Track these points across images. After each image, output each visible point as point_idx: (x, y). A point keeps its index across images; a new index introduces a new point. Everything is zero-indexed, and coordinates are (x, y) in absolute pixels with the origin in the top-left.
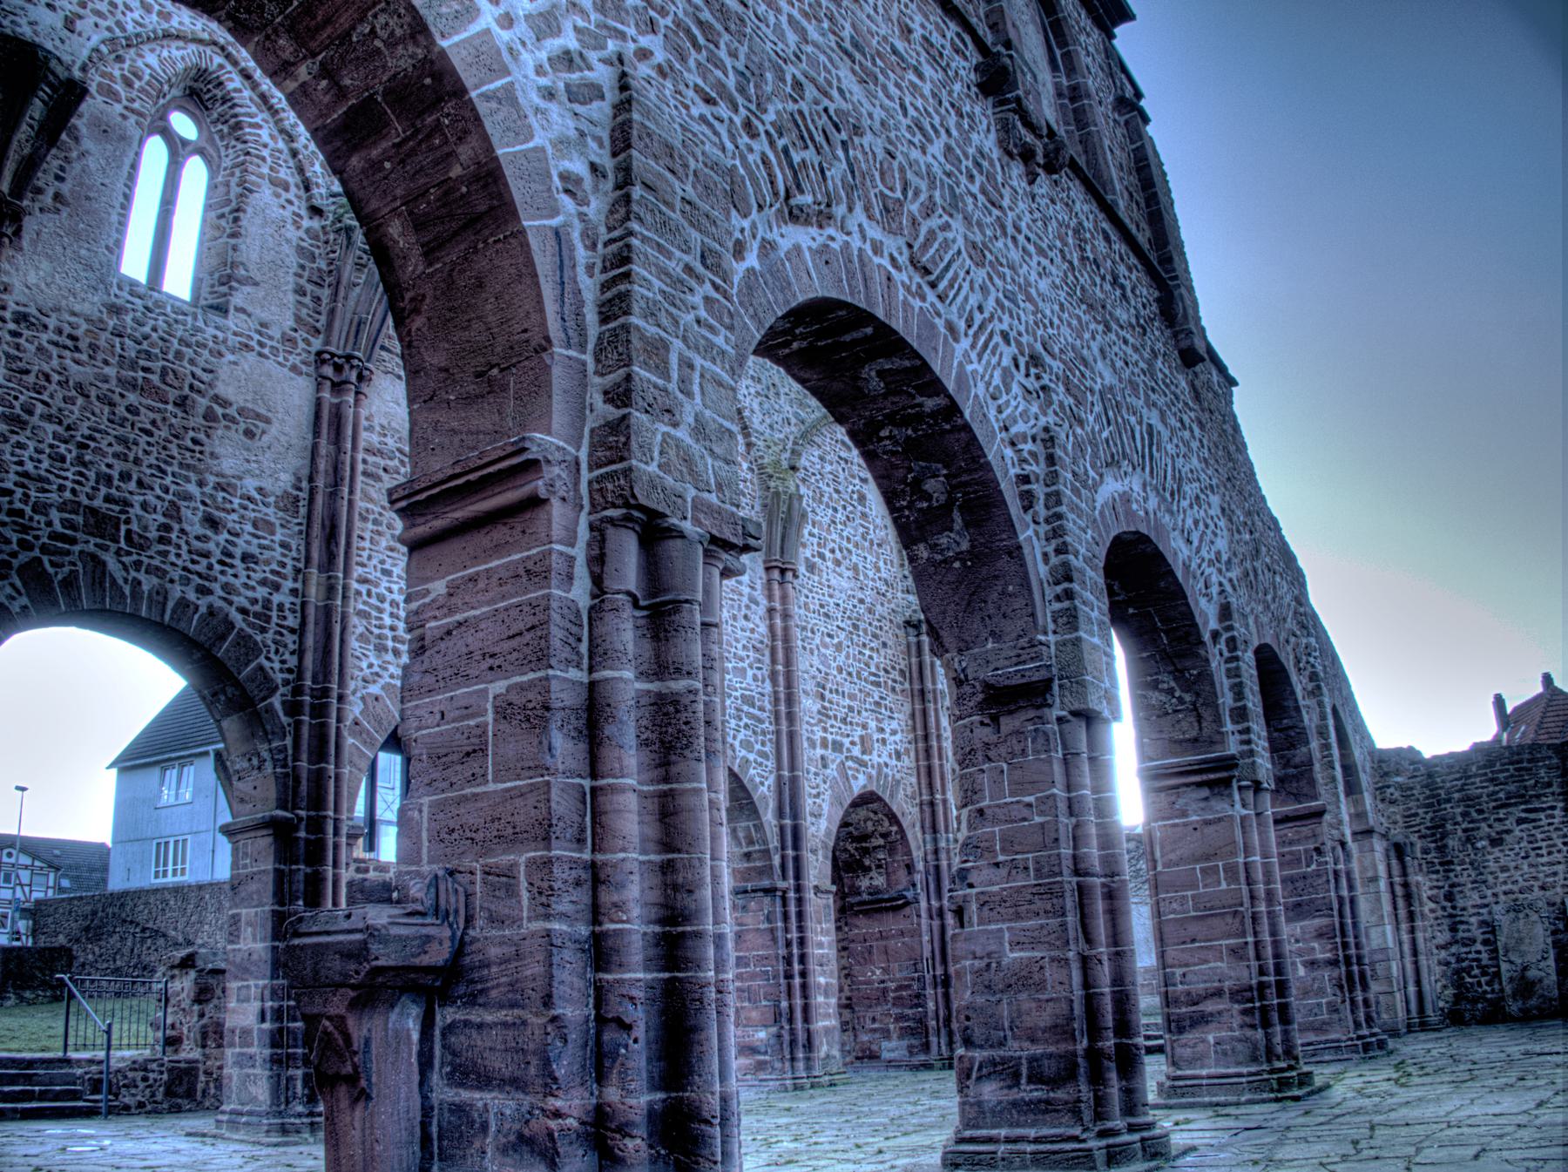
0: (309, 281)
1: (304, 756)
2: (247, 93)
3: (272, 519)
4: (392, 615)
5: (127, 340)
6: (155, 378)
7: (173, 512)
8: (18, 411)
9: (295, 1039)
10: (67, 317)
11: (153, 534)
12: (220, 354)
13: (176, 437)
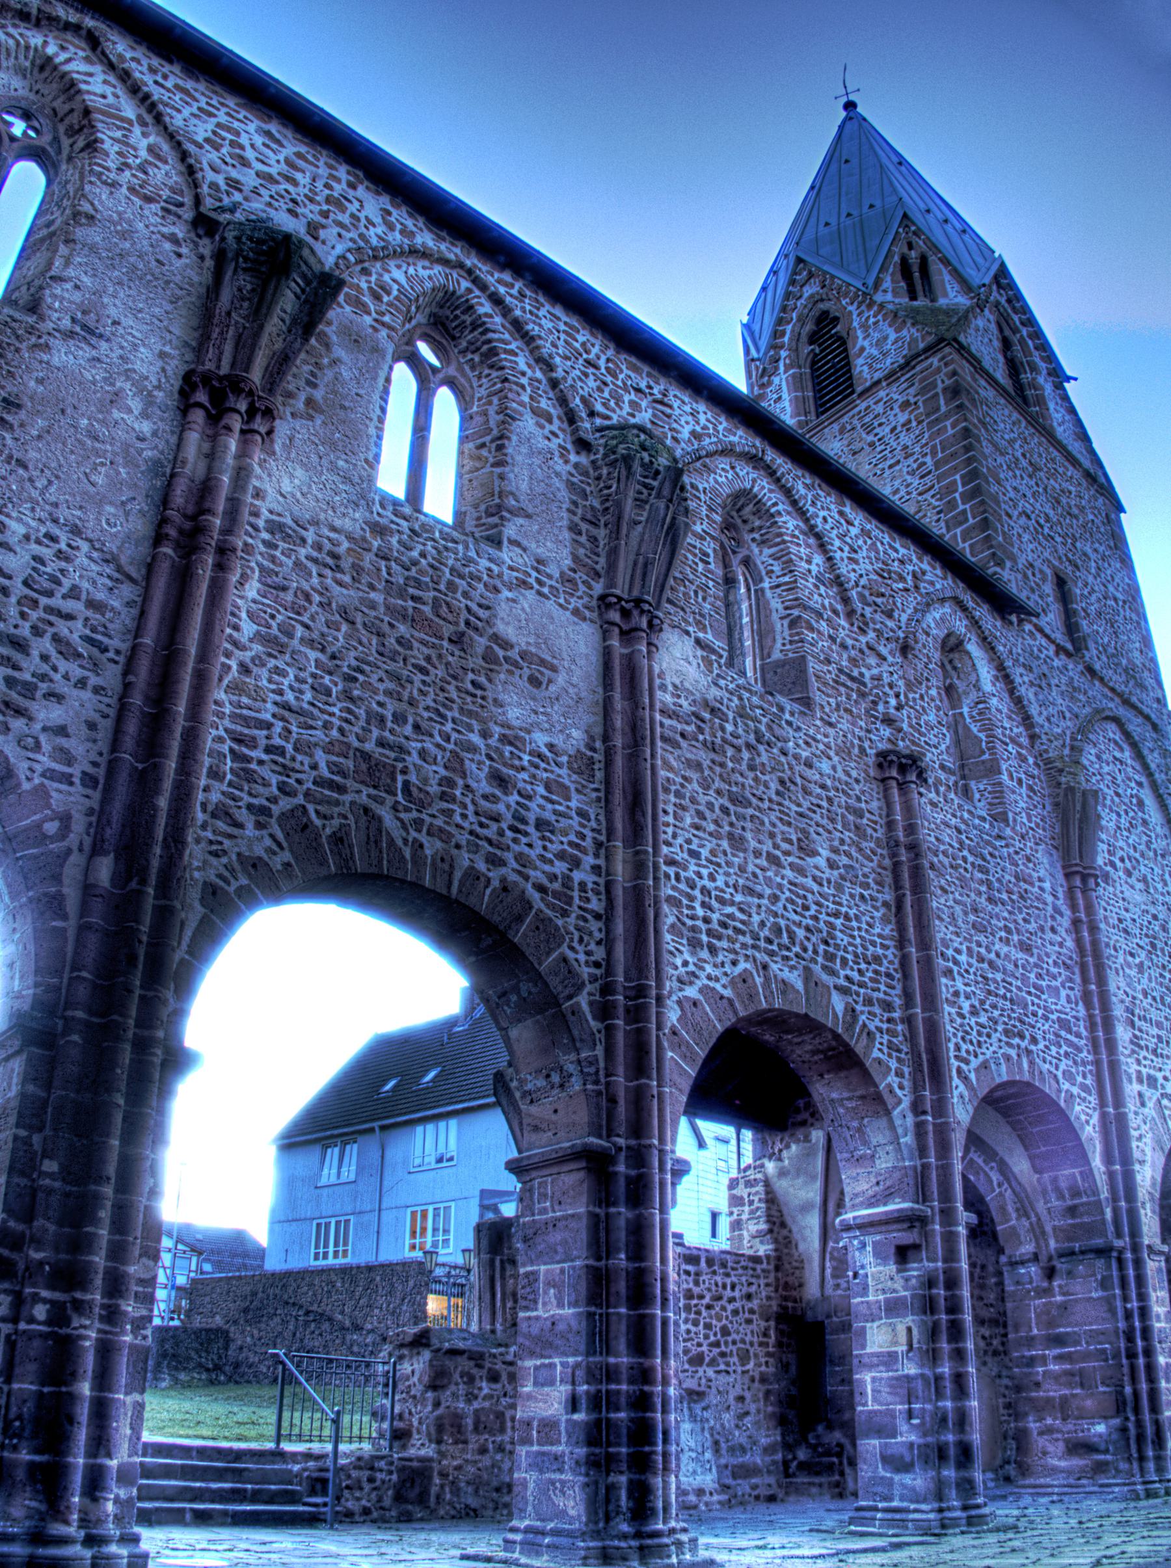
0: (583, 519)
1: (621, 1070)
2: (498, 319)
3: (567, 782)
4: (703, 904)
5: (393, 564)
6: (427, 609)
7: (456, 764)
8: (275, 631)
9: (618, 1436)
10: (326, 531)
11: (434, 789)
12: (496, 590)
13: (455, 678)
